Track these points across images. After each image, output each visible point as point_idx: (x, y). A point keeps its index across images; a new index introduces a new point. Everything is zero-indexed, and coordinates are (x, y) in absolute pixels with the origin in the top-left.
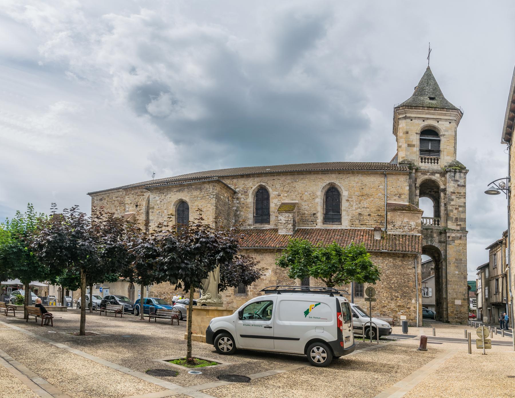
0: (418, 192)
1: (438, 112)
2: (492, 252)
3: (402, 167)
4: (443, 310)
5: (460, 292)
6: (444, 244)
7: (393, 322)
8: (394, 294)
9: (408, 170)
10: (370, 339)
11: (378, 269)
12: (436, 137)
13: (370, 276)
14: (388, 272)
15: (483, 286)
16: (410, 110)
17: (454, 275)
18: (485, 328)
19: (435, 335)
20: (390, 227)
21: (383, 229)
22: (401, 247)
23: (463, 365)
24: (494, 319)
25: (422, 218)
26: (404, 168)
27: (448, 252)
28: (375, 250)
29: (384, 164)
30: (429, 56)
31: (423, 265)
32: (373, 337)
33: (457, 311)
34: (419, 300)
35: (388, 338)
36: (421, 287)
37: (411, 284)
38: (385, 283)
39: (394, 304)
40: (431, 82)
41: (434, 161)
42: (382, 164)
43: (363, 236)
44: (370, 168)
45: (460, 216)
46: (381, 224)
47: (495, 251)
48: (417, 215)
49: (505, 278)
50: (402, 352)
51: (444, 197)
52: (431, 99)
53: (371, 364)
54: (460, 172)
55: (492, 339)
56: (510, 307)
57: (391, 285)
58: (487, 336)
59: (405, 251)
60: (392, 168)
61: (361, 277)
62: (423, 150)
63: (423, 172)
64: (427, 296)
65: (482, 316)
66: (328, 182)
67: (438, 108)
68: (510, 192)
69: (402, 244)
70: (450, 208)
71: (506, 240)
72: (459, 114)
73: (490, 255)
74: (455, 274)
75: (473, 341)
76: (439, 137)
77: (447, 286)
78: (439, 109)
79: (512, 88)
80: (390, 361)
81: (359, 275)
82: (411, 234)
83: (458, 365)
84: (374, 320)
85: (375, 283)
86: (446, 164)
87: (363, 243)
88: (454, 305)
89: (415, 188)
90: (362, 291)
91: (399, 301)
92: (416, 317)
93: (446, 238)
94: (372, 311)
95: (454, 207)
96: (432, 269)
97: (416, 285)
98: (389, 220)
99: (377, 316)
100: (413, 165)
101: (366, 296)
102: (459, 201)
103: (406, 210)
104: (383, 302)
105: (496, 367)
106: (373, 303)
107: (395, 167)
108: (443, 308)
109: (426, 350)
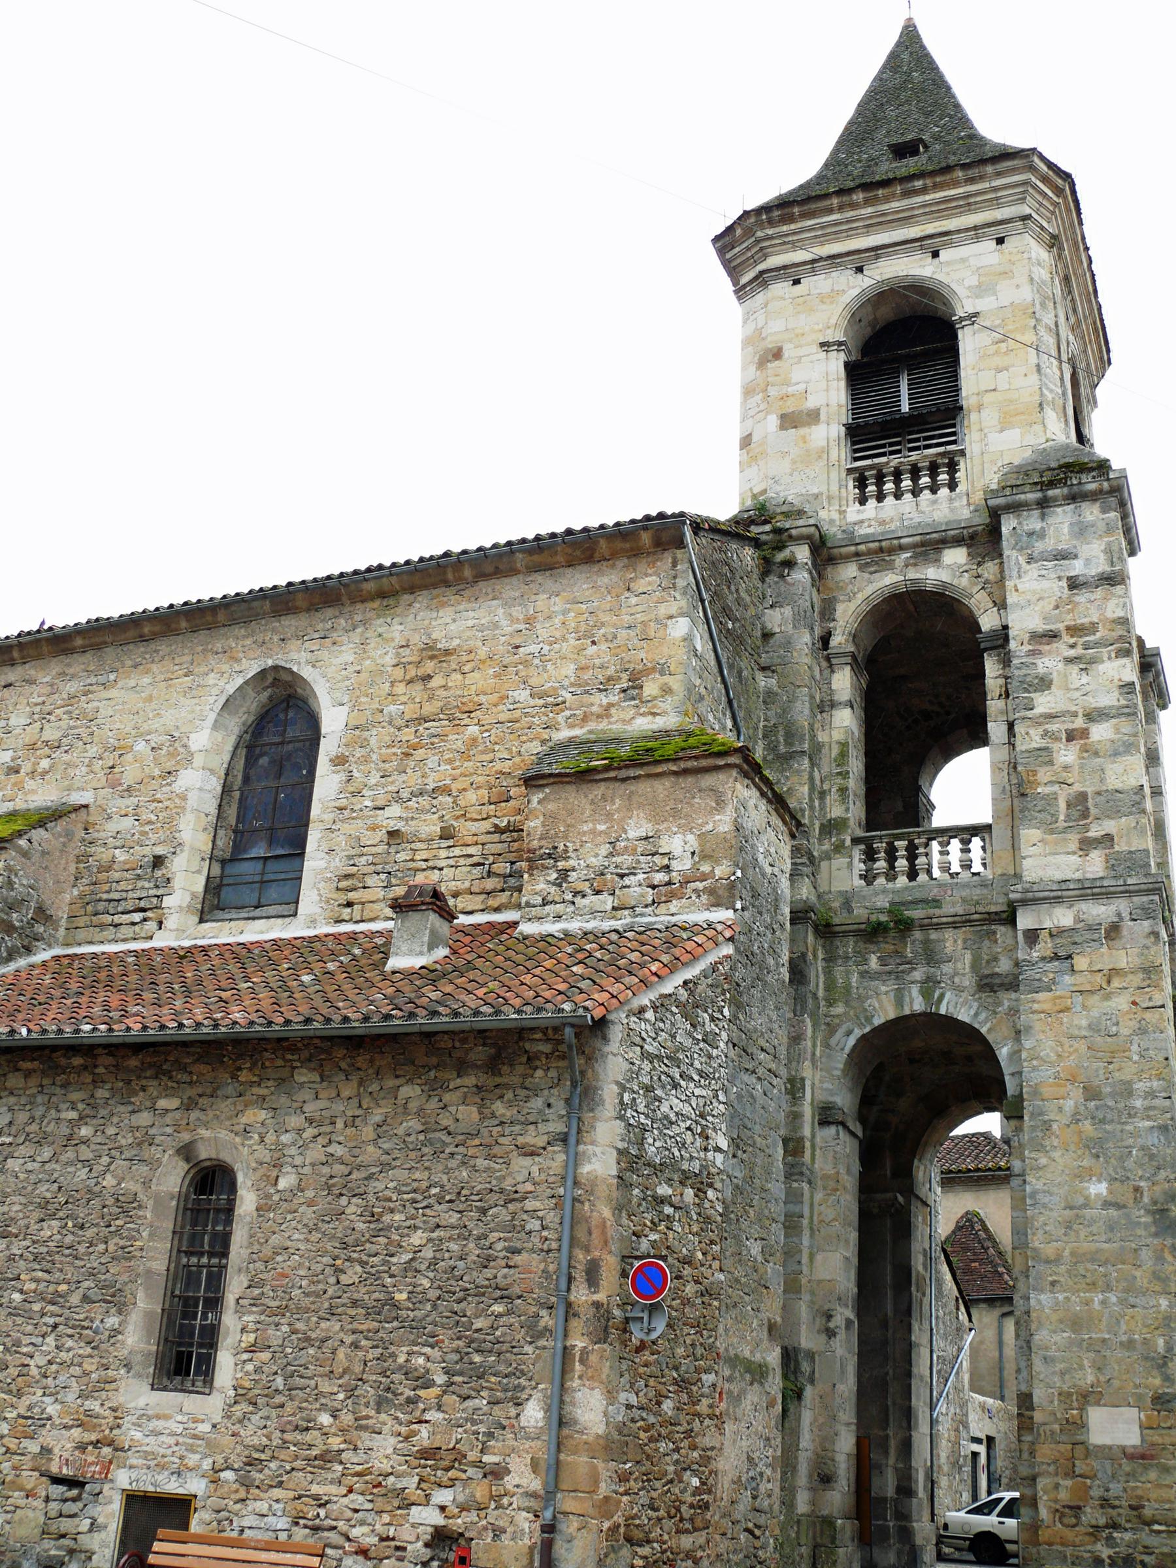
1: (927, 197)
5: (1129, 1345)
8: (401, 1359)
14: (380, 1186)
16: (785, 228)
39: (393, 1440)
48: (708, 780)
51: (1001, 681)
66: (253, 668)
78: (929, 182)
91: (433, 1415)
95: (1054, 727)
102: (1085, 679)
104: (325, 1419)
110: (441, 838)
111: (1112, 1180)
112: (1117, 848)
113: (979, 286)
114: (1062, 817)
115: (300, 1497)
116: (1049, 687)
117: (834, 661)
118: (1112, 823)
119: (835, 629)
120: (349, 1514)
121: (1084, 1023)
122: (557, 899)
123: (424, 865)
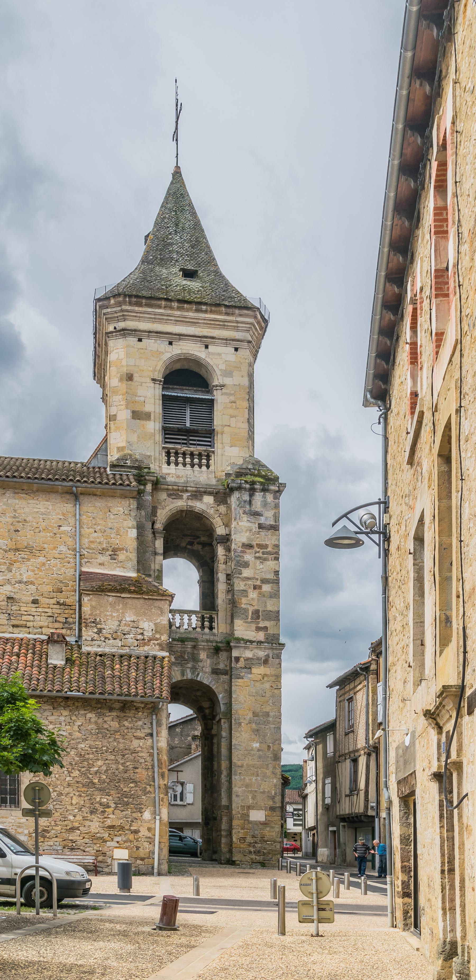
0: (159, 544)
2: (344, 694)
3: (118, 477)
4: (221, 835)
5: (264, 792)
6: (224, 677)
7: (96, 866)
8: (98, 800)
9: (134, 483)
10: (34, 906)
11: (57, 739)
12: (202, 391)
13: (37, 757)
14: (83, 746)
15: (320, 776)
17: (249, 752)
18: (320, 875)
19: (198, 894)
20: (88, 634)
21: (71, 639)
22: (116, 685)
23: (264, 962)
24: (344, 854)
25: (171, 611)
26: (125, 477)
27: (234, 696)
28: (49, 691)
29: (72, 465)
30: (177, 129)
31: (172, 728)
32: (41, 903)
33: (253, 836)
34: (160, 812)
35: (82, 903)
36: (166, 782)
37: (142, 774)
38: (76, 773)
39: (98, 823)
40: (186, 221)
41: (200, 459)
42: (67, 464)
43: (18, 655)
44: (35, 474)
45: (265, 606)
46: (66, 625)
47: (350, 690)
48: (158, 603)
49: (374, 755)
50: (114, 935)
52: (189, 274)
53: (35, 968)
54: (265, 490)
55: (337, 901)
56: (384, 825)
57: (90, 776)
58: (324, 893)
59: (126, 695)
60: (94, 478)
61: (12, 757)
62: (170, 427)
63: (173, 490)
64: (181, 803)
65: (315, 846)
67: (206, 304)
68: (387, 539)
69: (120, 678)
70: (239, 585)
71: (378, 664)
72: (258, 323)
73: (338, 700)
74: (252, 750)
75: (289, 905)
76: (209, 392)
77: (231, 778)
78: (209, 308)
79: (385, 233)
80: (83, 956)
81: (6, 753)
82: (143, 653)
83: (252, 963)
84: (45, 861)
85: (48, 773)
86: (229, 468)
87: (19, 673)
88: (246, 822)
89: (154, 533)
90: (15, 792)
92: (154, 853)
93: (231, 661)
94: (41, 839)
95: (250, 582)
96: (194, 738)
97: (154, 777)
98: (87, 617)
99: (54, 852)
100: (146, 470)
101: (25, 805)
102: (261, 567)
103: (130, 592)
104: (71, 818)
105: (343, 965)
106: (43, 822)
107: (101, 474)
108: (220, 830)
109: (175, 930)
110: (32, 603)
111: (261, 743)
112: (269, 632)
113: (225, 371)
114: (250, 617)
115: (65, 840)
116: (248, 567)
117: (157, 535)
118: (268, 622)
119: (157, 520)
120: (84, 845)
121: (254, 691)
122: (98, 639)
123: (26, 613)
